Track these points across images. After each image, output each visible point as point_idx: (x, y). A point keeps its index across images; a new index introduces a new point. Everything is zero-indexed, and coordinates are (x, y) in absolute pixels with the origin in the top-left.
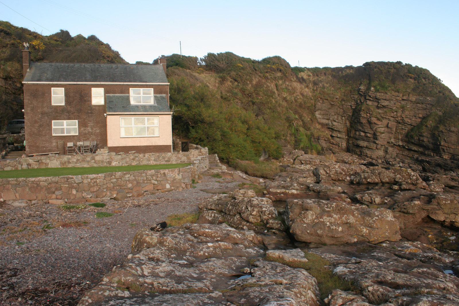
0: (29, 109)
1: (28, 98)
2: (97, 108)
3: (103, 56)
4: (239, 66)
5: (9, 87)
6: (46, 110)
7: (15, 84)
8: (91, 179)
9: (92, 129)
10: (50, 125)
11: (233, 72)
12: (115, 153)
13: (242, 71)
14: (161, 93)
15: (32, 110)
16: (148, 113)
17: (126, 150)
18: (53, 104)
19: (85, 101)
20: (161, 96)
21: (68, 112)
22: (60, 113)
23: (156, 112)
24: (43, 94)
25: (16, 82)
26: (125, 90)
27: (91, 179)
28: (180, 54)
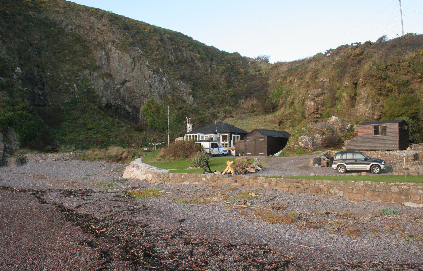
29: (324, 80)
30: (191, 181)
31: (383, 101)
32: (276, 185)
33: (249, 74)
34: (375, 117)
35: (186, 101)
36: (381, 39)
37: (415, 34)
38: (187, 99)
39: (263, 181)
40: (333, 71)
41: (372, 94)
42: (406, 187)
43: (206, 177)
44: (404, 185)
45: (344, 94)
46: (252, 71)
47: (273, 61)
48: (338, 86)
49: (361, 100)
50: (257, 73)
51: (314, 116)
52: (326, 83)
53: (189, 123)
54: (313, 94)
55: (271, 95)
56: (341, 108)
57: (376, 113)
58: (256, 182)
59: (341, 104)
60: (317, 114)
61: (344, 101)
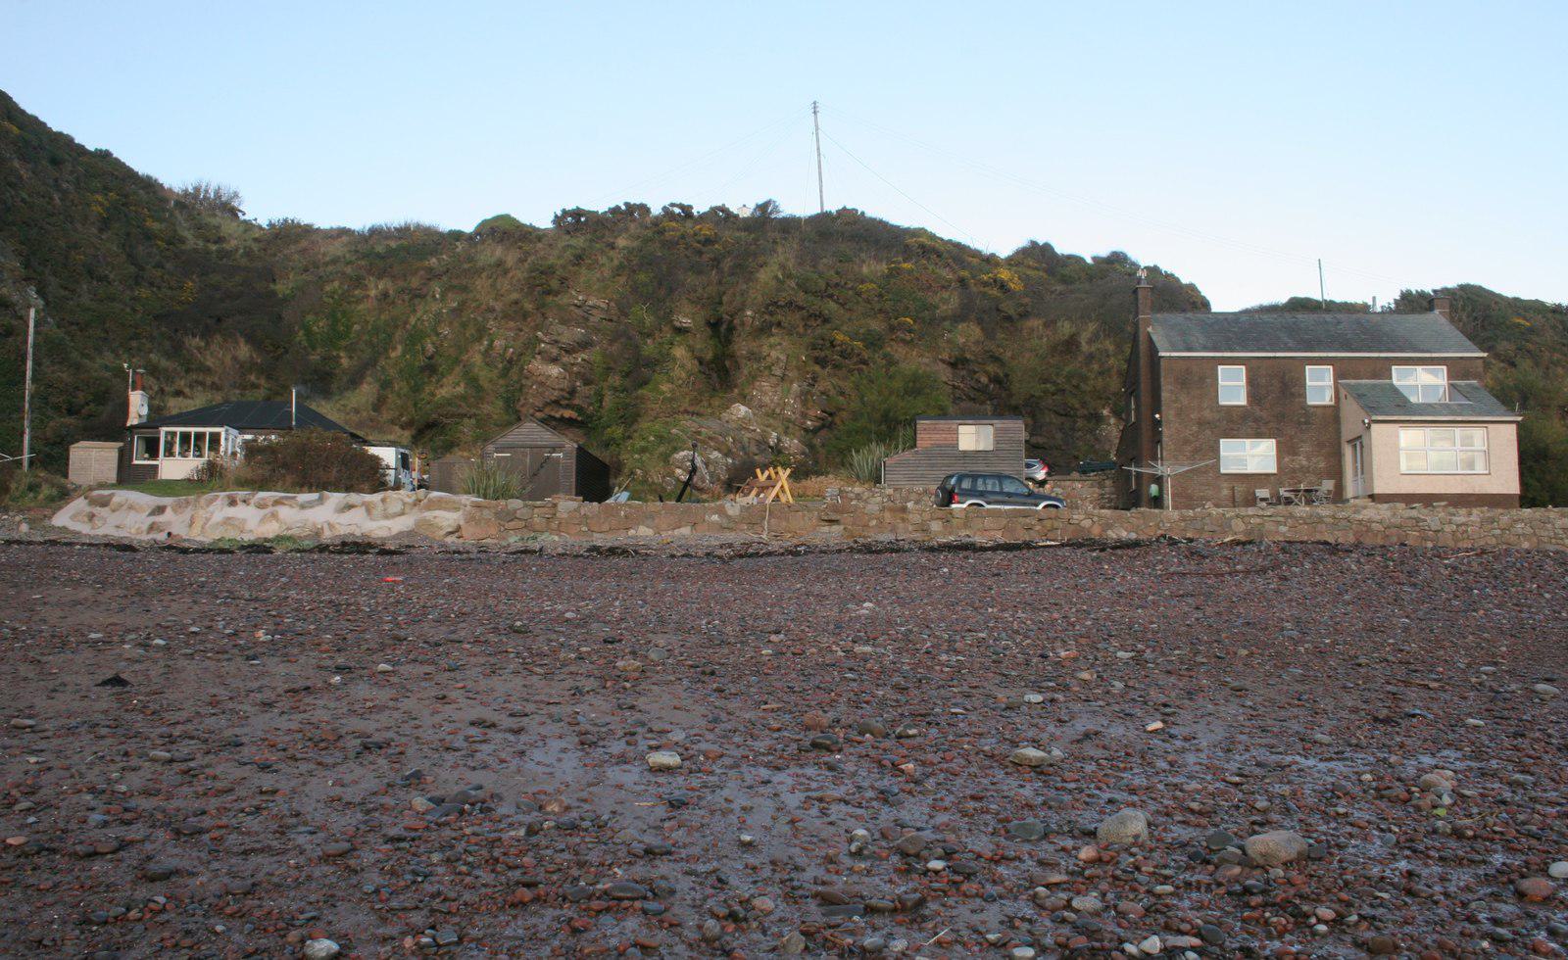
0: (1172, 412)
1: (1170, 387)
2: (1319, 411)
3: (1194, 303)
4: (1519, 324)
5: (962, 386)
6: (1207, 414)
7: (976, 376)
8: (1458, 526)
9: (1308, 459)
10: (1215, 450)
11: (1505, 343)
12: (1403, 505)
13: (1535, 338)
14: (1465, 376)
15: (1179, 413)
16: (1459, 418)
17: (1409, 499)
18: (1223, 402)
19: (1292, 394)
20: (1466, 385)
21: (1256, 420)
22: (1240, 424)
23: (1480, 415)
24: (1202, 379)
25: (975, 372)
26: (1382, 369)
27: (1458, 526)
28: (1319, 298)
29: (590, 303)
30: (664, 526)
31: (827, 382)
32: (966, 526)
33: (183, 247)
34: (809, 423)
35: (14, 305)
36: (763, 208)
37: (863, 213)
38: (15, 298)
39: (926, 516)
40: (622, 280)
41: (798, 358)
42: (1258, 520)
43: (721, 511)
44: (1253, 516)
45: (679, 352)
46: (192, 241)
47: (261, 209)
48: (648, 324)
49: (767, 372)
50: (214, 248)
51: (553, 414)
52: (594, 312)
53: (134, 389)
54: (556, 342)
55: (301, 333)
56: (672, 391)
57: (811, 413)
58: (903, 520)
59: (671, 380)
60: (567, 407)
61: (678, 373)
